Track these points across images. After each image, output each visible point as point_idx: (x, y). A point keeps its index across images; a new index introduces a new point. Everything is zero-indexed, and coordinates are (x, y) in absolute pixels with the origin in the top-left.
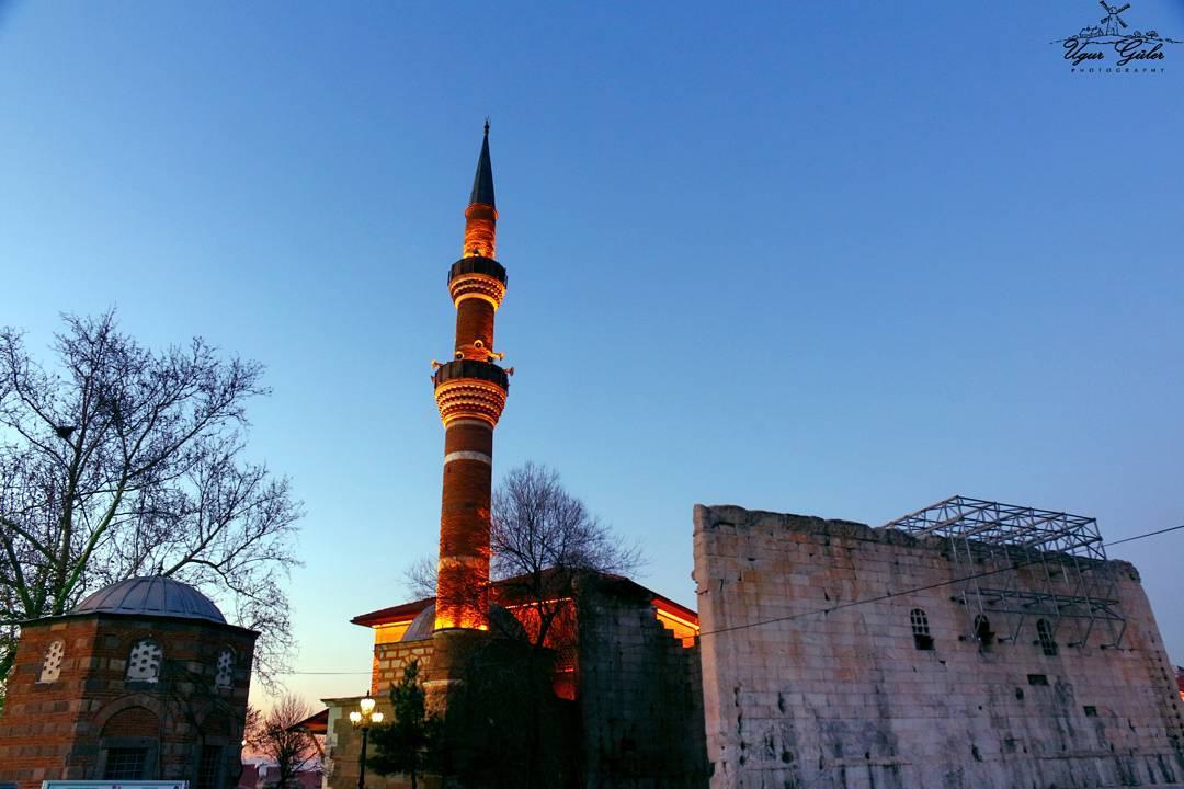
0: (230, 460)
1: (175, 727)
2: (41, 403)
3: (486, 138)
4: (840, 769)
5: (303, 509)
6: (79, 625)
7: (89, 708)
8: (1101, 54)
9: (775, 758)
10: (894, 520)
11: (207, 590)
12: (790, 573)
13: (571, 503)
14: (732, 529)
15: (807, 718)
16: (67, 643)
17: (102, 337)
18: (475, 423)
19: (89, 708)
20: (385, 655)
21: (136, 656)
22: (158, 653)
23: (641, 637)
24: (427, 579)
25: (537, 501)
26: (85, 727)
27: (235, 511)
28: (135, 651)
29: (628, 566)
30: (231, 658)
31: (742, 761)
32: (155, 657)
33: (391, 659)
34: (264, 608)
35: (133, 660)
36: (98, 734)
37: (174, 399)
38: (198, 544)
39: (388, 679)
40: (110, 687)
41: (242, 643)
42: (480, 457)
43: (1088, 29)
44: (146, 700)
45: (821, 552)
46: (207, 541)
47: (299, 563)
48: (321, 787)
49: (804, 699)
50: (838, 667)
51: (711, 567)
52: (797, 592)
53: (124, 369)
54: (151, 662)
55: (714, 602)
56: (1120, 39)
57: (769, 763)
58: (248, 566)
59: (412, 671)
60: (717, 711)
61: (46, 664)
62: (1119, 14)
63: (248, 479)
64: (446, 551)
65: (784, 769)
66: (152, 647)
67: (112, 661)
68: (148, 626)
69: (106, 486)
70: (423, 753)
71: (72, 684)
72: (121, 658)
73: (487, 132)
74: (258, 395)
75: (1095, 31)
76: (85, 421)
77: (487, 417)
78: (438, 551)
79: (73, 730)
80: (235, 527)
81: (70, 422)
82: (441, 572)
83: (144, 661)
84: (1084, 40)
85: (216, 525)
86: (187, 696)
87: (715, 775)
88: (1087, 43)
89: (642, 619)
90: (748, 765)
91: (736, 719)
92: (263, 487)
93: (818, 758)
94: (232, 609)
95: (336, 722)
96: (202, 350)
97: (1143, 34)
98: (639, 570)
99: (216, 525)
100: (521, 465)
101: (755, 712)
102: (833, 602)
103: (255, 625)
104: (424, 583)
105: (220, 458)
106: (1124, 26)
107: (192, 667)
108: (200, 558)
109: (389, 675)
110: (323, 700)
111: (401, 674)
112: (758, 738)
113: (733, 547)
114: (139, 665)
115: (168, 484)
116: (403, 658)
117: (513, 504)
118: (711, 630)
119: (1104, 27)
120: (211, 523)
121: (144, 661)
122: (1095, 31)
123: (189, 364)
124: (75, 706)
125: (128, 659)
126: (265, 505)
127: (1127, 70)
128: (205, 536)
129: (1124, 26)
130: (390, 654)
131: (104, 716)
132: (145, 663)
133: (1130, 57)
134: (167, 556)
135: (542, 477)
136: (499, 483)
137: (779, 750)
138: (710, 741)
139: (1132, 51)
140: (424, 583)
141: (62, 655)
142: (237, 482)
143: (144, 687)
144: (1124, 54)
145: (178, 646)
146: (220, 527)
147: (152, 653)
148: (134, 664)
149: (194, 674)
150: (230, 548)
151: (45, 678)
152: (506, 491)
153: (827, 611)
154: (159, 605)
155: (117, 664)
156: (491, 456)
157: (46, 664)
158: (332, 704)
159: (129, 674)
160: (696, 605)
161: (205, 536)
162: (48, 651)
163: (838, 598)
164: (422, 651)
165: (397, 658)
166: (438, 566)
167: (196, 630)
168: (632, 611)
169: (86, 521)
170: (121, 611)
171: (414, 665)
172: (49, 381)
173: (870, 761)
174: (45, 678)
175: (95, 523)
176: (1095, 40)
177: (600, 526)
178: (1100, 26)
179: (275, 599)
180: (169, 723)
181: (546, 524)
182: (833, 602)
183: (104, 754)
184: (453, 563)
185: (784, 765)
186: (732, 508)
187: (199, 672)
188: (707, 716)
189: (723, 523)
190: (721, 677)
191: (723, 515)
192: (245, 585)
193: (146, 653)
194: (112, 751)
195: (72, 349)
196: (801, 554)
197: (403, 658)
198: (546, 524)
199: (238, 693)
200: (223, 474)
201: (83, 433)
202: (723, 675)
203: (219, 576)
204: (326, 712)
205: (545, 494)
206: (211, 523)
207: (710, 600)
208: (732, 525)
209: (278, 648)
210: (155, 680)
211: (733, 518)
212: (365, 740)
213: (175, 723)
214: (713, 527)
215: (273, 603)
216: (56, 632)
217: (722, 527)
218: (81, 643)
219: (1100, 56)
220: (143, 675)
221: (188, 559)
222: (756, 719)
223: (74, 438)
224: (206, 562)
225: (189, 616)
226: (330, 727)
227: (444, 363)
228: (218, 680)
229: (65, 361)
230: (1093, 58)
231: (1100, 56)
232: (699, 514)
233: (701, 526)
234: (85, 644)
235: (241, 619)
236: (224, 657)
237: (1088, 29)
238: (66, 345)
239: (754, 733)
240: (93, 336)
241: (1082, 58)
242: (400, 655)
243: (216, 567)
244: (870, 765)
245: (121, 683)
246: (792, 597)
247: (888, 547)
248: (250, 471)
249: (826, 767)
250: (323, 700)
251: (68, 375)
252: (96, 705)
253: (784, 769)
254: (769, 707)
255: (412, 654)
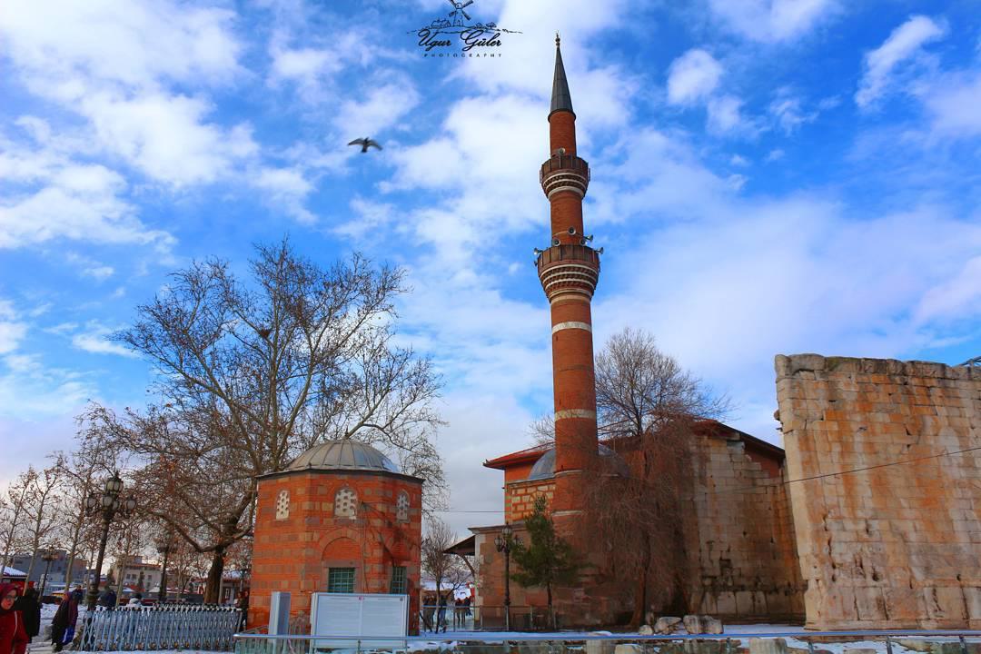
0: (385, 345)
1: (372, 553)
2: (246, 313)
3: (558, 50)
4: (931, 589)
5: (443, 380)
6: (297, 478)
7: (312, 539)
8: (449, 42)
9: (865, 577)
10: (974, 357)
11: (378, 446)
12: (870, 412)
13: (664, 360)
14: (812, 374)
15: (894, 542)
16: (291, 491)
17: (282, 258)
18: (575, 297)
19: (312, 539)
20: (516, 492)
21: (339, 500)
22: (354, 498)
23: (732, 471)
24: (548, 429)
25: (635, 359)
26: (310, 552)
27: (393, 384)
28: (338, 497)
29: (719, 412)
30: (406, 500)
31: (834, 579)
32: (352, 501)
33: (521, 495)
34: (420, 460)
35: (338, 503)
36: (321, 557)
37: (343, 302)
38: (367, 413)
39: (520, 511)
40: (324, 523)
41: (413, 485)
42: (582, 325)
43: (438, 21)
44: (350, 533)
45: (900, 391)
46: (373, 410)
47: (444, 423)
48: (978, 645)
49: (890, 525)
50: (924, 496)
51: (794, 409)
52: (878, 429)
53: (303, 280)
54: (350, 504)
55: (799, 440)
56: (464, 29)
57: (858, 581)
58: (406, 427)
59: (540, 504)
60: (808, 536)
61: (278, 507)
62: (464, 9)
63: (400, 358)
64: (560, 404)
65: (875, 587)
66: (350, 493)
67: (323, 504)
68: (345, 477)
69: (298, 372)
70: (555, 570)
71: (298, 521)
72: (331, 502)
73: (558, 44)
74: (403, 294)
75: (444, 23)
76: (276, 325)
77: (584, 291)
78: (553, 406)
79: (303, 554)
80: (394, 396)
81: (267, 325)
82: (556, 422)
83: (345, 504)
84: (435, 30)
85: (379, 397)
86: (378, 529)
87: (809, 591)
88: (437, 33)
89: (731, 455)
90: (839, 582)
91: (826, 543)
92: (411, 366)
93: (907, 578)
94: (397, 461)
95: (482, 546)
96: (361, 261)
97: (484, 25)
98: (729, 414)
99: (379, 397)
100: (620, 331)
101: (843, 536)
102: (915, 437)
103: (416, 473)
104: (546, 433)
105: (377, 343)
106: (468, 19)
107: (380, 507)
108: (370, 423)
109: (521, 508)
110: (469, 529)
111: (530, 507)
112: (849, 558)
113: (814, 390)
114: (342, 507)
115: (344, 368)
116: (531, 495)
117: (614, 364)
118: (866, 466)
119: (451, 20)
120: (375, 395)
121: (345, 504)
122: (444, 23)
123: (350, 273)
124: (303, 537)
125: (335, 504)
126: (414, 378)
127: (470, 55)
128: (372, 405)
129: (468, 19)
130: (520, 491)
131: (322, 544)
132: (346, 506)
133: (473, 44)
134: (345, 422)
135: (639, 341)
136: (600, 346)
137: (868, 571)
138: (802, 562)
139: (474, 40)
140: (546, 433)
141: (288, 500)
142: (391, 362)
143: (347, 523)
144: (468, 41)
145: (368, 492)
146: (382, 397)
147: (350, 498)
148: (339, 506)
149: (382, 513)
150: (391, 413)
151: (279, 516)
152: (608, 354)
153: (908, 446)
154: (349, 461)
155: (327, 507)
156: (590, 324)
157: (278, 507)
158: (477, 532)
159: (336, 513)
160: (783, 442)
161: (372, 405)
162: (279, 498)
163: (920, 433)
164: (545, 488)
165: (526, 494)
166: (554, 418)
167: (380, 478)
168: (723, 449)
169: (287, 401)
170: (324, 467)
171: (543, 500)
172: (250, 297)
173: (962, 582)
174: (279, 516)
175: (294, 401)
176: (445, 30)
177: (692, 378)
178: (448, 18)
179: (428, 452)
180: (369, 551)
181: (643, 378)
182: (915, 437)
183: (327, 571)
184: (564, 414)
185: (874, 583)
186: (811, 355)
187: (385, 511)
188: (799, 540)
189: (802, 370)
190: (810, 506)
191: (803, 363)
192: (405, 441)
193: (346, 498)
194: (331, 570)
195: (263, 271)
196: (881, 396)
197: (531, 495)
198: (643, 378)
199: (413, 526)
200: (380, 356)
201: (277, 333)
202: (812, 504)
203: (386, 437)
204: (474, 537)
205: (642, 354)
206: (375, 395)
207: (796, 438)
208: (812, 371)
209: (435, 491)
210: (355, 518)
211: (813, 365)
212: (508, 560)
213: (372, 549)
214: (793, 375)
215: (427, 456)
216: (282, 483)
217: (802, 373)
218: (301, 491)
219: (448, 43)
220: (346, 514)
221: (361, 424)
222: (846, 542)
223: (272, 336)
224: (375, 426)
225: (374, 469)
226: (477, 549)
227: (544, 249)
228: (399, 516)
229: (259, 280)
230: (442, 45)
231: (448, 43)
232: (781, 363)
233: (782, 373)
234: (303, 493)
235: (405, 469)
236: (401, 499)
237: (438, 21)
238: (257, 268)
239: (842, 553)
240: (277, 259)
241: (433, 45)
242: (528, 492)
243: (382, 429)
244: (962, 587)
245: (332, 520)
246: (873, 433)
247: (969, 383)
248: (400, 353)
249: (914, 587)
250: (469, 529)
251: (262, 290)
252: (316, 536)
253: (875, 587)
254: (857, 532)
255: (537, 490)
